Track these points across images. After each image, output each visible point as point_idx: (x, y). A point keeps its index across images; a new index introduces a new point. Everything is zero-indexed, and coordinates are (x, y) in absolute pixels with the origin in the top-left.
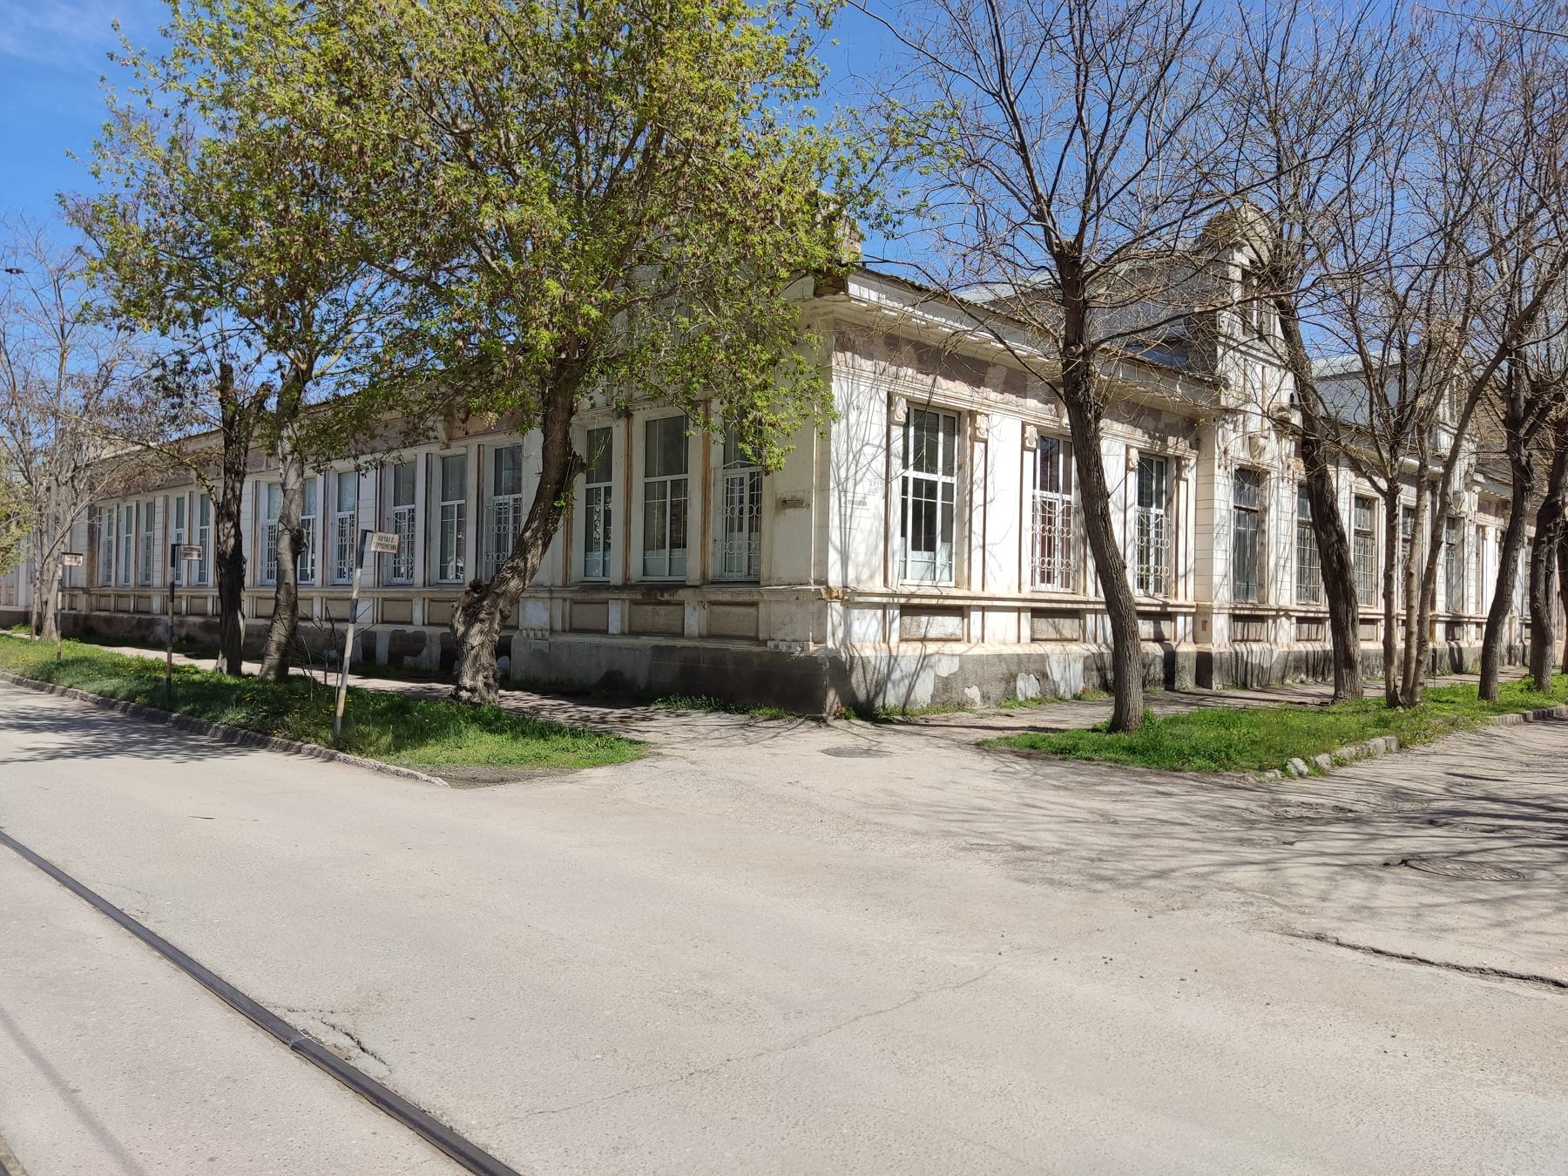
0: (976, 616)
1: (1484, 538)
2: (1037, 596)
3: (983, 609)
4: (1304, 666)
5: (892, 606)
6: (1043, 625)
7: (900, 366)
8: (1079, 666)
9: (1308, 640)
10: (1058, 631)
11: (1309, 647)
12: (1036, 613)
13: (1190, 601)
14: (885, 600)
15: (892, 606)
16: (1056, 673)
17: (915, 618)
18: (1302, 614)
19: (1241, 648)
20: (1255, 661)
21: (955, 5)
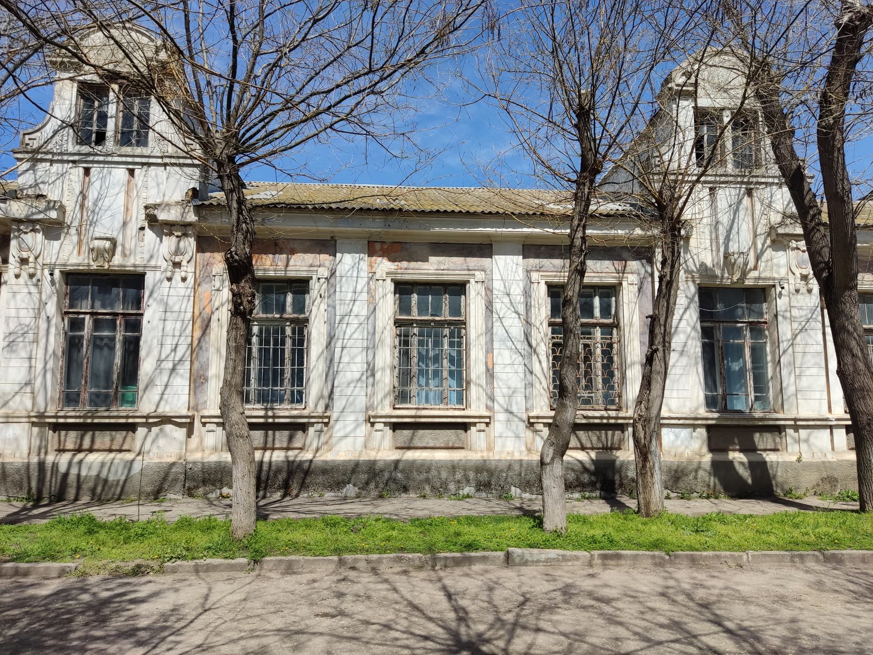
15: (839, 427)
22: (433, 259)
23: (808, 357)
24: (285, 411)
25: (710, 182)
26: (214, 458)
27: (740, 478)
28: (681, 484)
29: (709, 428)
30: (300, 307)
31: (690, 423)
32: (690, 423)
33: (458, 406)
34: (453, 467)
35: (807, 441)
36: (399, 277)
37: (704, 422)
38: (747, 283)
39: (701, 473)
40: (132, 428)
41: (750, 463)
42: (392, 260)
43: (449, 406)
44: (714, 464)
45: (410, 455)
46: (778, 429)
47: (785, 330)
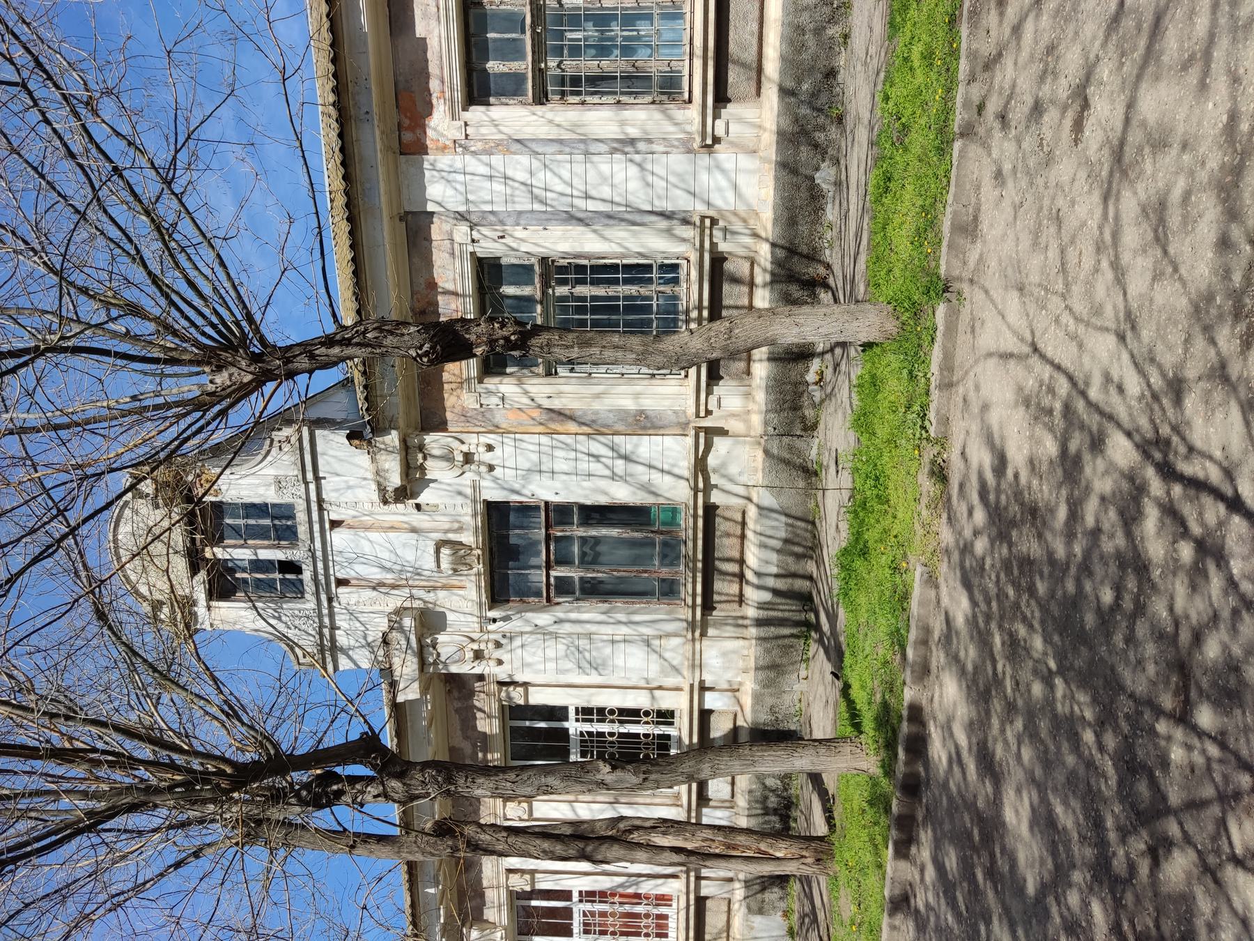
22: (420, 31)
30: (522, 273)
36: (459, 96)
40: (711, 511)
42: (429, 109)
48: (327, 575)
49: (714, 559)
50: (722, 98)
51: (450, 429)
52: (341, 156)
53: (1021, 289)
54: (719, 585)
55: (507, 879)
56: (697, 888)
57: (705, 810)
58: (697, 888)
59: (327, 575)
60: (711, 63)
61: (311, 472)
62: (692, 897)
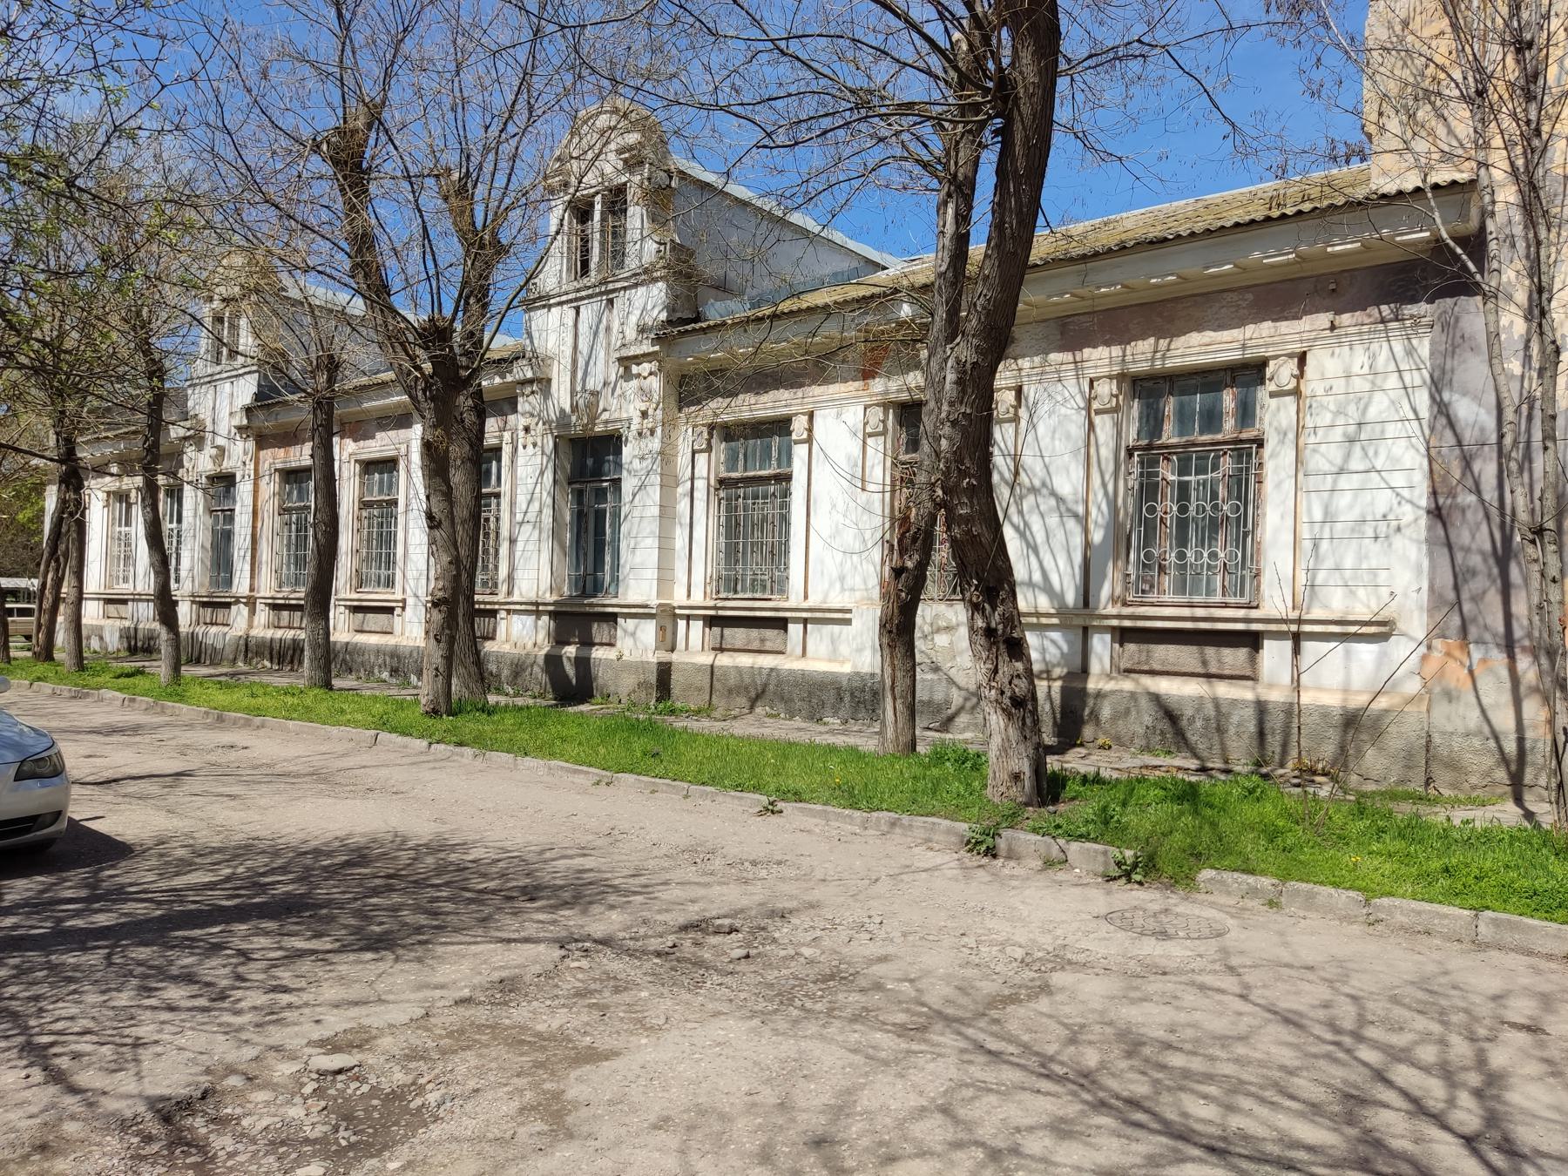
0: (795, 630)
1: (720, 372)
2: (720, 604)
3: (805, 621)
4: (267, 653)
5: (696, 617)
6: (112, 608)
7: (1338, 312)
8: (117, 635)
9: (290, 628)
10: (1205, 663)
11: (279, 634)
12: (109, 601)
13: (698, 598)
14: (805, 615)
15: (696, 617)
16: (107, 638)
17: (1144, 647)
18: (712, 613)
19: (200, 630)
20: (210, 642)
21: (532, 1)
22: (379, 435)
23: (645, 523)
24: (378, 596)
25: (571, 301)
26: (95, 622)
27: (567, 676)
28: (519, 681)
29: (554, 615)
30: (1246, 413)
31: (535, 609)
32: (535, 609)
33: (731, 595)
34: (378, 651)
35: (633, 634)
36: (364, 457)
37: (1115, 623)
38: (597, 429)
39: (536, 669)
40: (227, 605)
41: (576, 658)
42: (355, 441)
43: (1197, 599)
44: (548, 657)
45: (724, 660)
46: (613, 618)
47: (628, 485)
48: (582, 298)
49: (722, 627)
50: (711, 622)
51: (262, 453)
52: (1394, 192)
53: (370, 790)
54: (285, 614)
55: (1009, 389)
56: (796, 620)
57: (1108, 637)
58: (796, 620)
59: (582, 298)
60: (1240, 626)
61: (645, 276)
62: (788, 614)
